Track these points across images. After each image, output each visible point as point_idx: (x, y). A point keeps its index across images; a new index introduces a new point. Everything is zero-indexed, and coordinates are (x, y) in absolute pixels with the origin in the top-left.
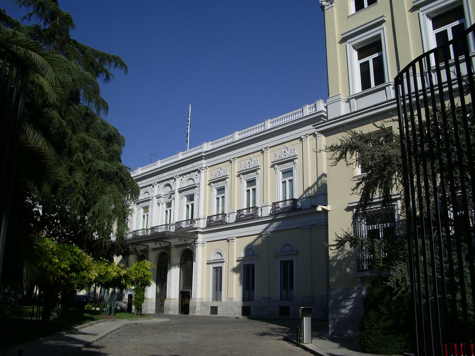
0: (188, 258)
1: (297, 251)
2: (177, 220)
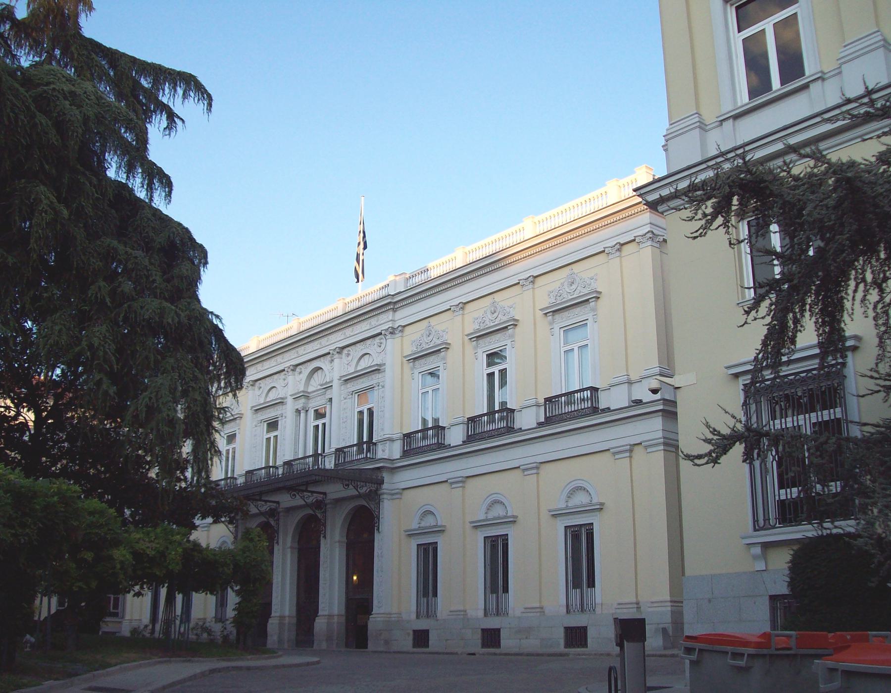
0: (363, 526)
1: (602, 504)
2: (335, 445)
